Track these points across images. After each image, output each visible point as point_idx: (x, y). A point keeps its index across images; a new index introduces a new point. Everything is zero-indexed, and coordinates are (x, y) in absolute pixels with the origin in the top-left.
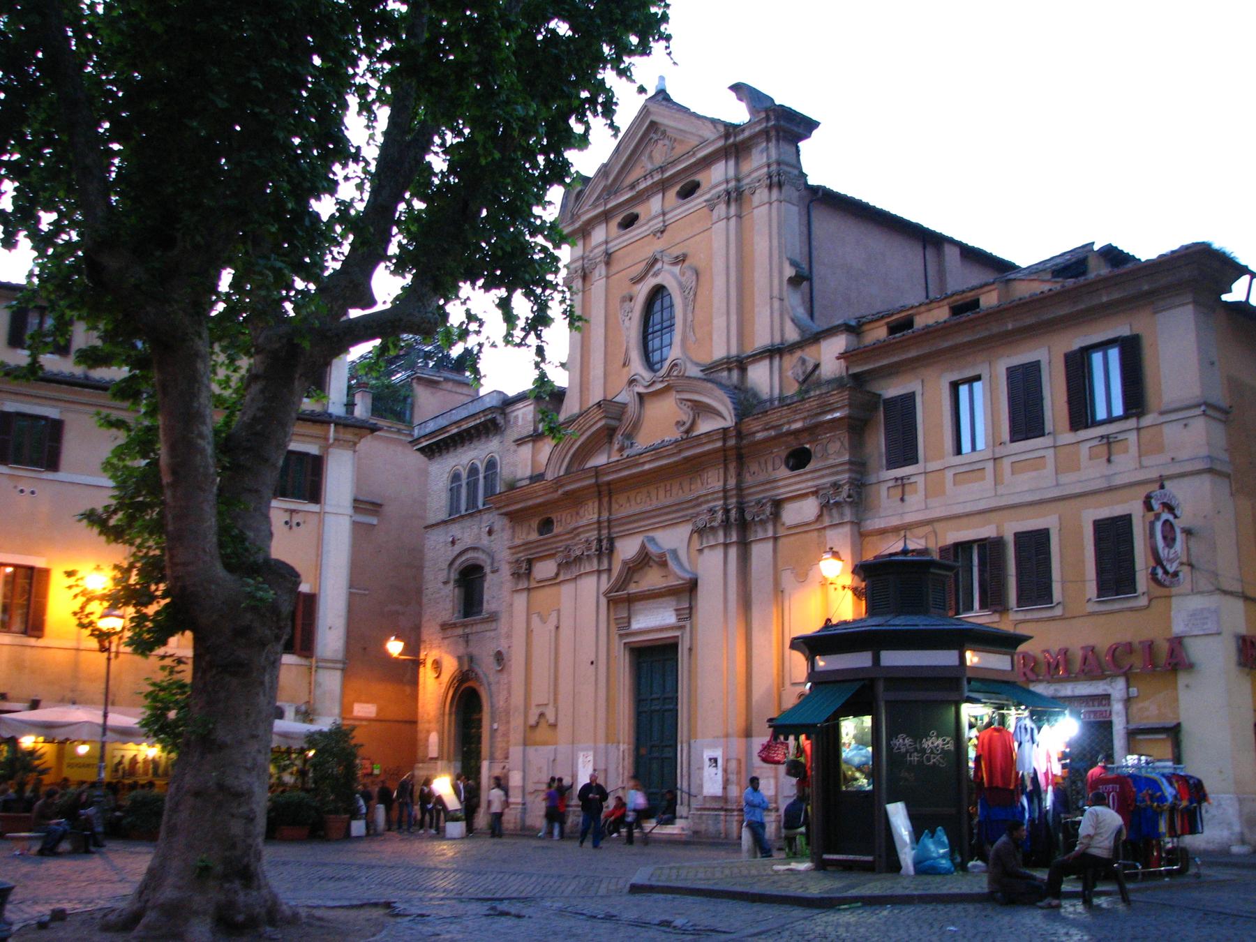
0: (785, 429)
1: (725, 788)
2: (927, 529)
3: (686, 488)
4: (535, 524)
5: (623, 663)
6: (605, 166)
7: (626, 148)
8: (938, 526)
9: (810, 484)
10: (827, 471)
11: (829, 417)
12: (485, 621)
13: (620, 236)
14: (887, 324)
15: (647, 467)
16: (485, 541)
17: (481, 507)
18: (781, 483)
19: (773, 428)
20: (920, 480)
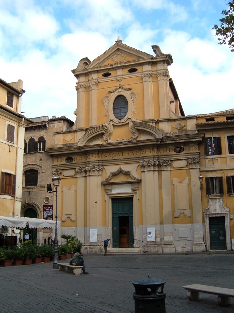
0: (178, 141)
1: (166, 233)
2: (222, 172)
3: (168, 151)
4: (65, 158)
5: (109, 203)
6: (99, 57)
7: (107, 54)
8: (224, 171)
9: (186, 157)
10: (59, 166)
11: (194, 140)
12: (39, 187)
13: (103, 78)
14: (206, 119)
15: (122, 146)
16: (38, 162)
17: (27, 153)
18: (173, 156)
19: (174, 141)
20: (219, 159)
